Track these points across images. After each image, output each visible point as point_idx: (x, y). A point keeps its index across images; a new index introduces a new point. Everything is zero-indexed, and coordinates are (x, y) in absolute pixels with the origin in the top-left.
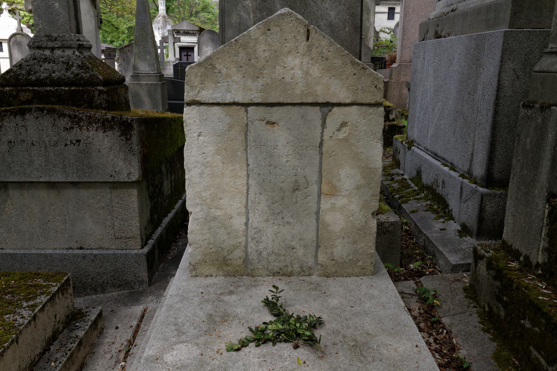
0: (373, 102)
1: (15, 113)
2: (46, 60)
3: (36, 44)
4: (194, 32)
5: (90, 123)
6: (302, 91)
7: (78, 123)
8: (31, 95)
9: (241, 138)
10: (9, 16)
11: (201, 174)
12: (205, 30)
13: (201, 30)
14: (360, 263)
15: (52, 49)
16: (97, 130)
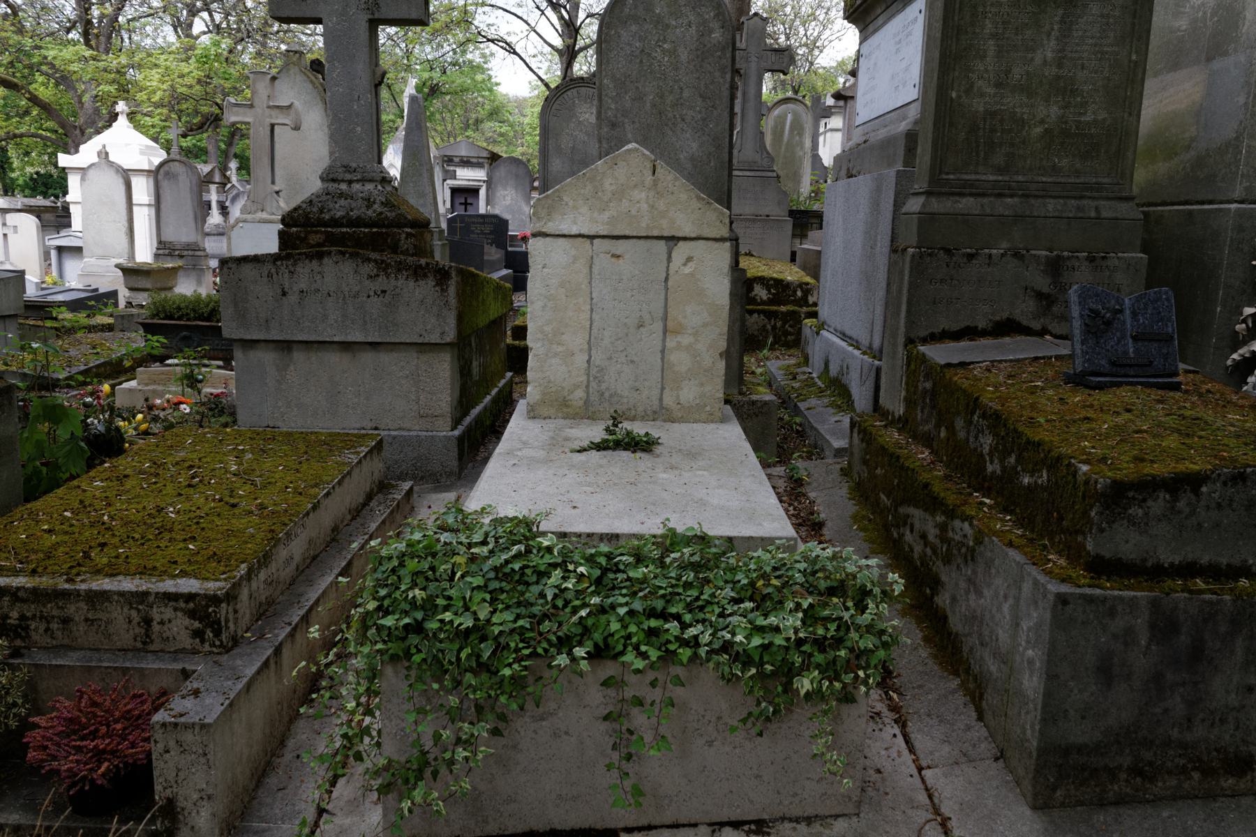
0: (718, 236)
1: (310, 257)
2: (341, 195)
3: (331, 176)
4: (480, 160)
5: (399, 270)
6: (648, 225)
7: (385, 270)
8: (323, 237)
9: (586, 270)
10: (128, 127)
11: (544, 307)
13: (494, 158)
14: (708, 408)
15: (350, 182)
16: (407, 279)
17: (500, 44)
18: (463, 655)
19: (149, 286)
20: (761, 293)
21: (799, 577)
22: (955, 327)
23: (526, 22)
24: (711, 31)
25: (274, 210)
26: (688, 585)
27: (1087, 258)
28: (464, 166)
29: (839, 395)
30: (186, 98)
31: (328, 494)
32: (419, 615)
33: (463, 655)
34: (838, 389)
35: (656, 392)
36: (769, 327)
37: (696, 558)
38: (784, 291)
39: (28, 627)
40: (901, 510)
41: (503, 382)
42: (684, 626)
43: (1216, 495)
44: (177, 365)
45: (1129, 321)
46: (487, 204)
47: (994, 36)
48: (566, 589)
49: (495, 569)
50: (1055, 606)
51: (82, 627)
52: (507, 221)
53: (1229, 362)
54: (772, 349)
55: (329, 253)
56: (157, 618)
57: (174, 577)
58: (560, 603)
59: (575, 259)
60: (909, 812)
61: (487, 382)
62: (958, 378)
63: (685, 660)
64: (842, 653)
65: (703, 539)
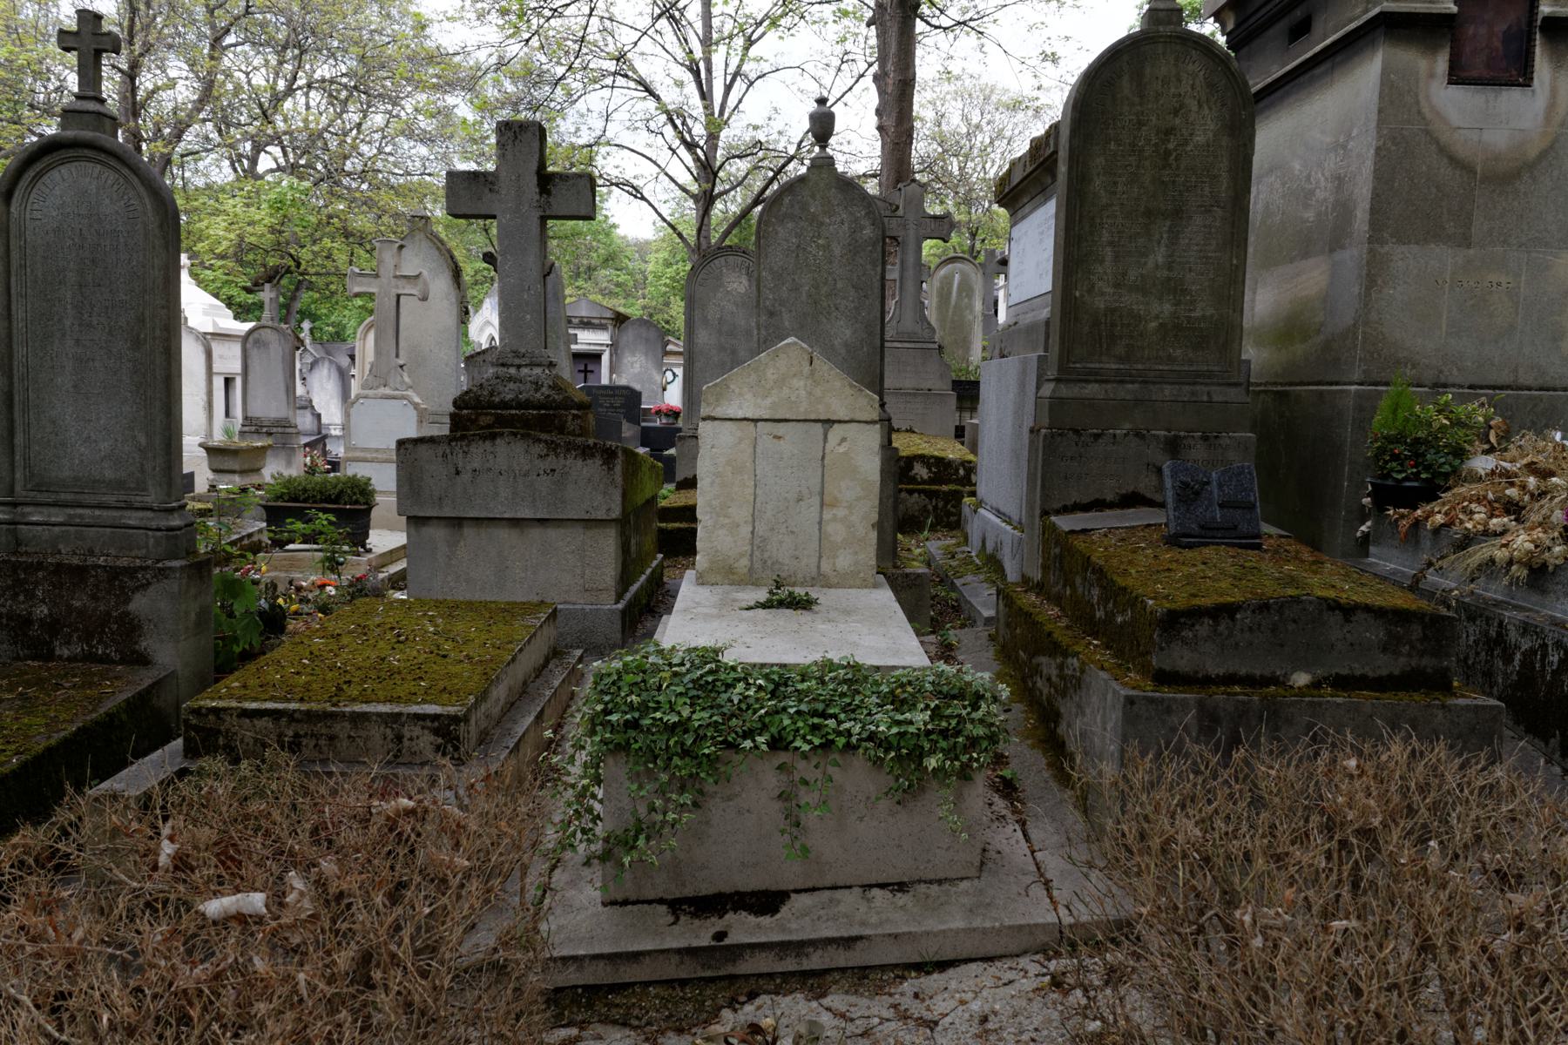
1: (484, 438)
2: (511, 379)
5: (568, 450)
7: (554, 450)
8: (493, 419)
11: (712, 483)
12: (629, 318)
15: (519, 367)
17: (626, 188)
18: (672, 743)
19: (237, 467)
20: (921, 471)
21: (928, 687)
22: (1086, 500)
23: (655, 163)
24: (862, 228)
25: (398, 386)
26: (843, 695)
27: (1202, 438)
28: (584, 328)
29: (995, 571)
30: (253, 248)
31: (521, 650)
32: (636, 715)
33: (672, 743)
34: (993, 563)
35: (814, 560)
36: (930, 507)
37: (850, 676)
38: (945, 470)
39: (300, 743)
40: (1034, 661)
41: (655, 563)
42: (840, 723)
43: (1247, 621)
44: (316, 550)
45: (1216, 491)
46: (611, 373)
47: (1111, 243)
48: (748, 696)
49: (693, 681)
50: (1125, 706)
51: (345, 743)
52: (640, 393)
53: (1359, 534)
54: (933, 529)
55: (502, 434)
56: (407, 735)
57: (418, 703)
58: (744, 706)
59: (741, 440)
60: (1020, 877)
61: (642, 562)
62: (1079, 543)
63: (840, 746)
64: (960, 739)
65: (856, 667)
